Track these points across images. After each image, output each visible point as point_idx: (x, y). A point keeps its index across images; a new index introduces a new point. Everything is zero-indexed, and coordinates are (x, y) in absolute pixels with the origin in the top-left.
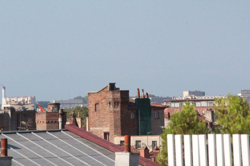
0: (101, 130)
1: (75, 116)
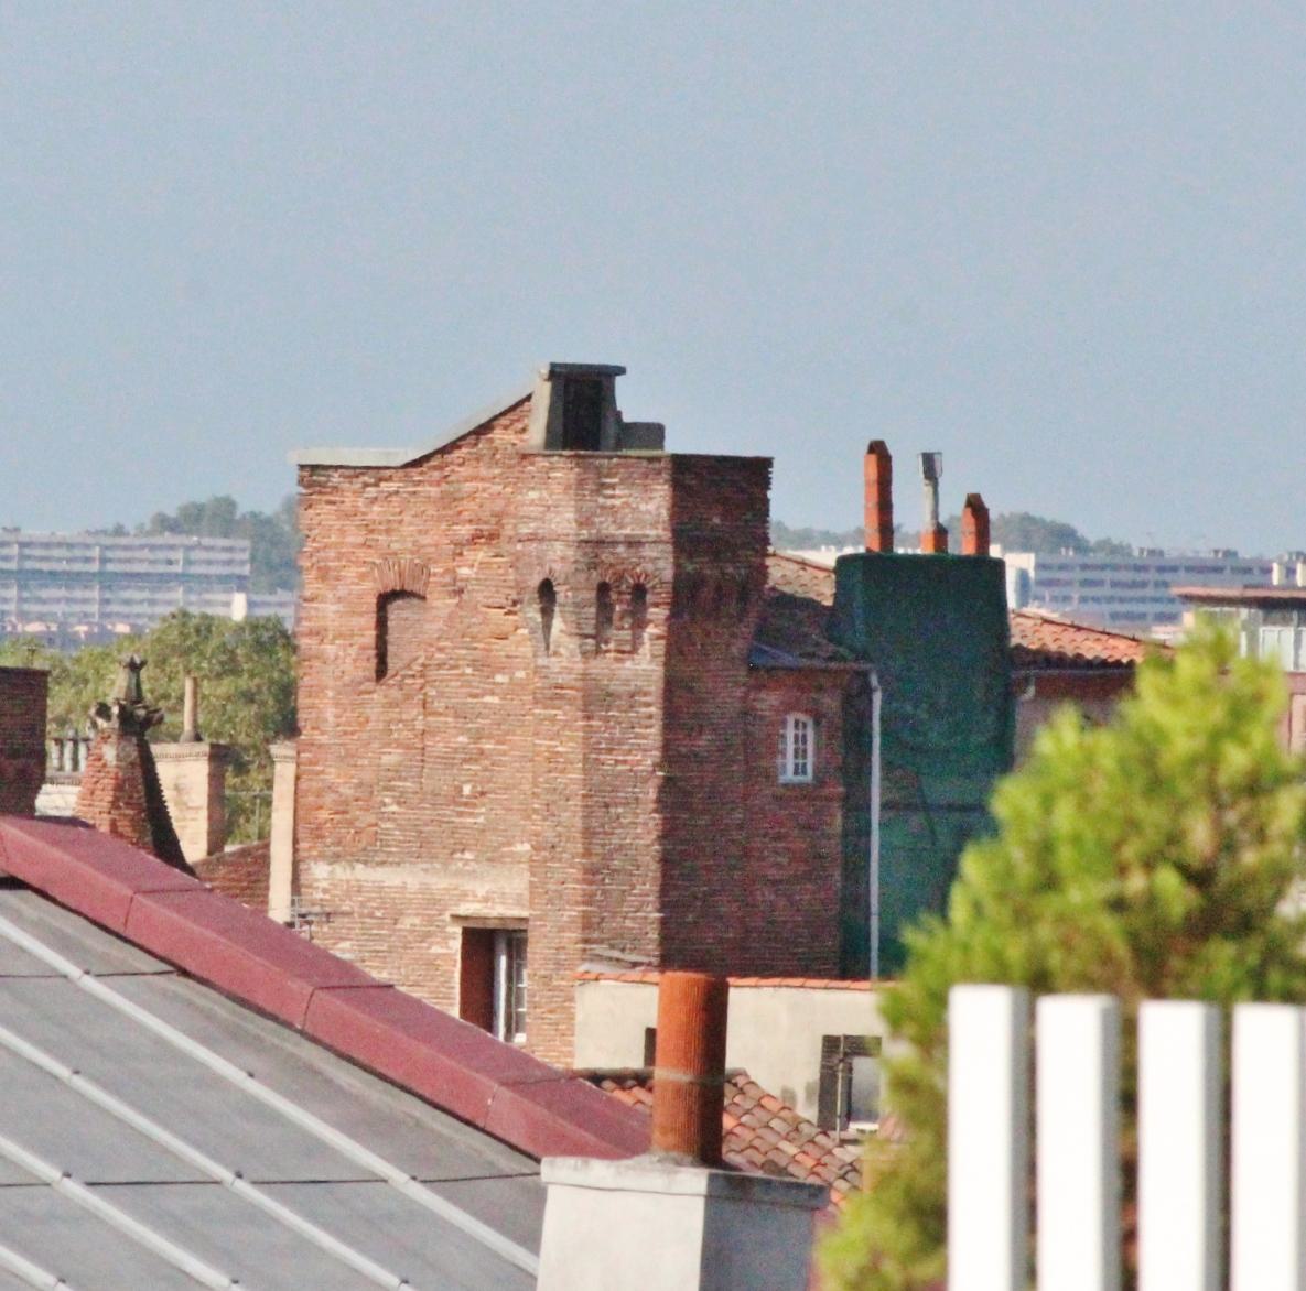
0: (431, 903)
1: (138, 725)
